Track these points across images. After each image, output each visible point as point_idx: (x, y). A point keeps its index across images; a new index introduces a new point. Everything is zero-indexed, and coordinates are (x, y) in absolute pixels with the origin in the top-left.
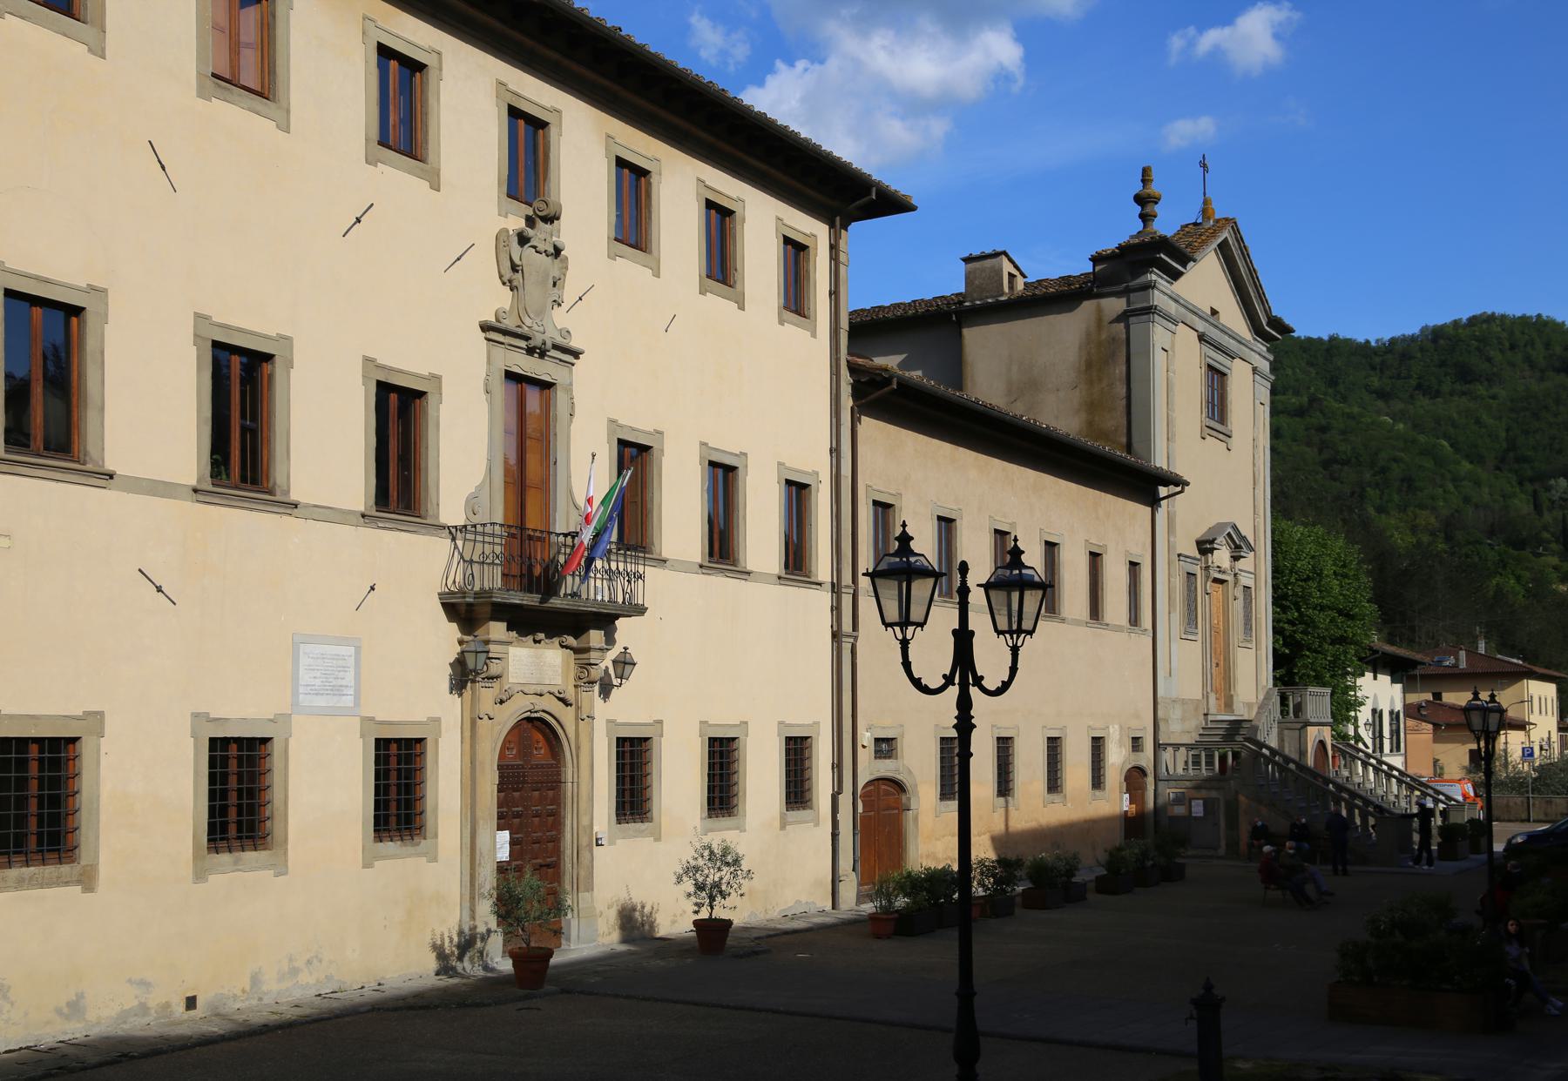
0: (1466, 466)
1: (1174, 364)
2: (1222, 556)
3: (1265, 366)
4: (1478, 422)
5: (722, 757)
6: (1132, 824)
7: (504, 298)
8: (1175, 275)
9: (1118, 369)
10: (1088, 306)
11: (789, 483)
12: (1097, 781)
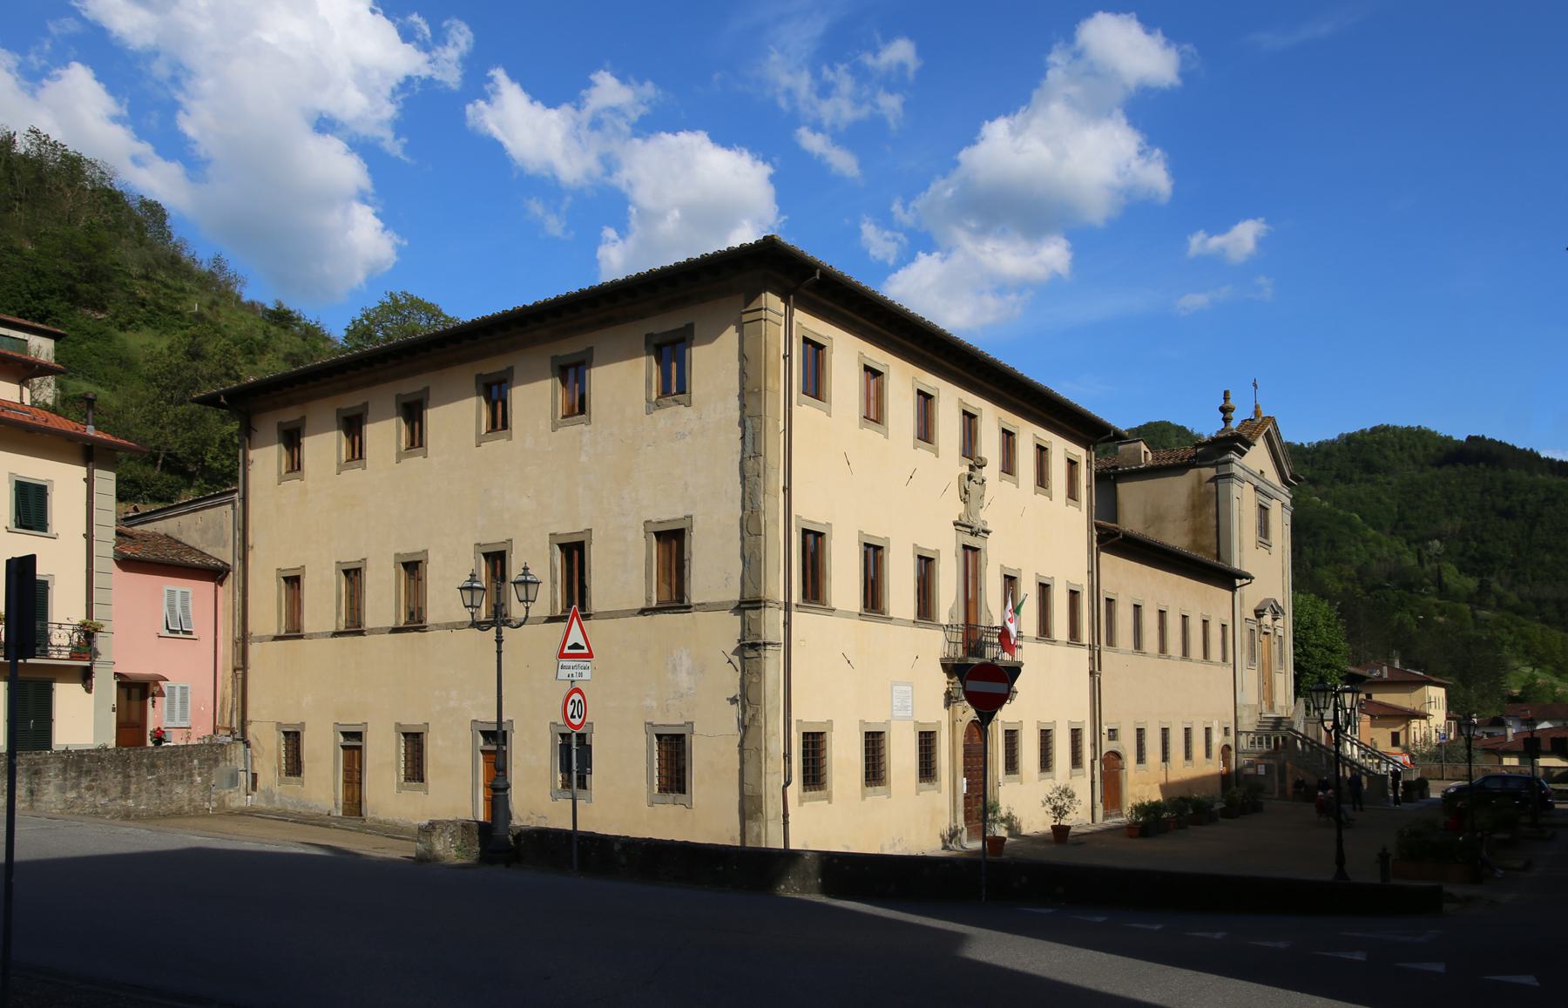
0: (1371, 532)
1: (1242, 503)
3: (1288, 502)
4: (1379, 500)
5: (874, 743)
6: (1226, 779)
7: (960, 508)
8: (1242, 453)
9: (1210, 511)
10: (1193, 472)
11: (920, 557)
12: (1208, 755)
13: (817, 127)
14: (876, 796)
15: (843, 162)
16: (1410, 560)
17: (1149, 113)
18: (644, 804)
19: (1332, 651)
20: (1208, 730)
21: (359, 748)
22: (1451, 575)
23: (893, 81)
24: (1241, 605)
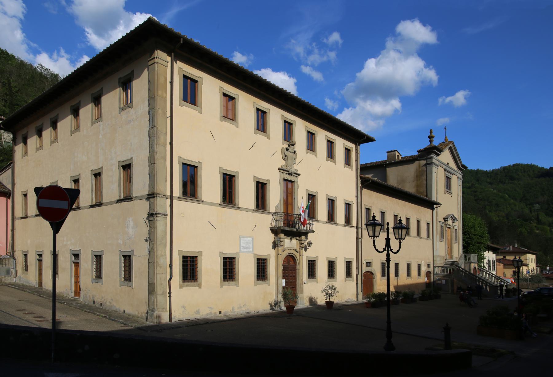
0: (512, 201)
1: (438, 176)
2: (450, 222)
3: (461, 176)
6: (428, 285)
7: (283, 163)
8: (438, 155)
9: (424, 177)
10: (417, 163)
13: (307, 65)
14: (229, 286)
15: (317, 76)
16: (527, 211)
17: (425, 52)
18: (118, 286)
19: (482, 237)
20: (419, 266)
21: (78, 263)
22: (543, 217)
23: (334, 47)
24: (437, 215)
